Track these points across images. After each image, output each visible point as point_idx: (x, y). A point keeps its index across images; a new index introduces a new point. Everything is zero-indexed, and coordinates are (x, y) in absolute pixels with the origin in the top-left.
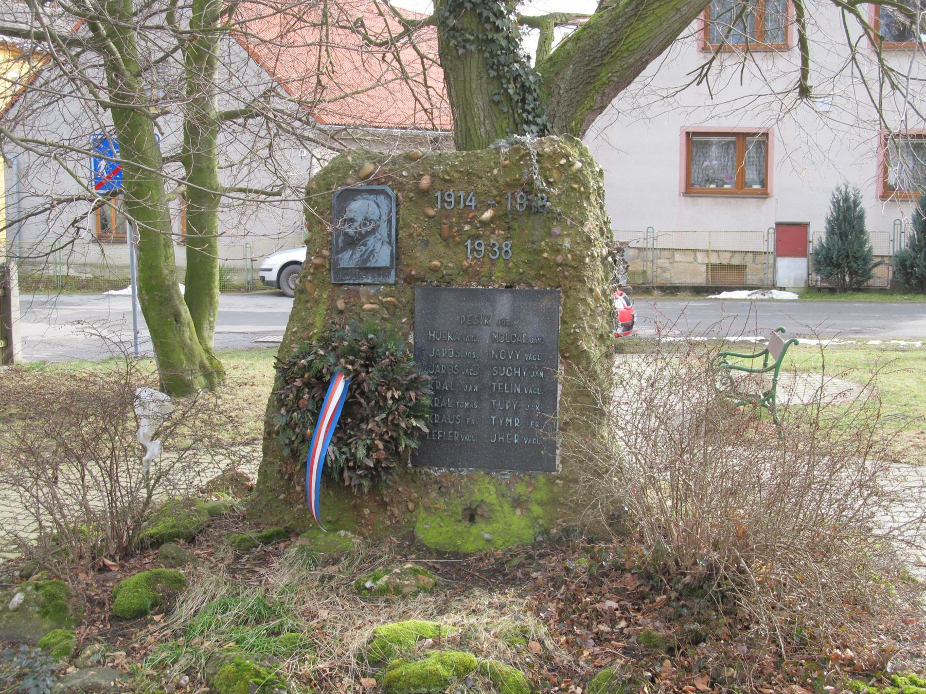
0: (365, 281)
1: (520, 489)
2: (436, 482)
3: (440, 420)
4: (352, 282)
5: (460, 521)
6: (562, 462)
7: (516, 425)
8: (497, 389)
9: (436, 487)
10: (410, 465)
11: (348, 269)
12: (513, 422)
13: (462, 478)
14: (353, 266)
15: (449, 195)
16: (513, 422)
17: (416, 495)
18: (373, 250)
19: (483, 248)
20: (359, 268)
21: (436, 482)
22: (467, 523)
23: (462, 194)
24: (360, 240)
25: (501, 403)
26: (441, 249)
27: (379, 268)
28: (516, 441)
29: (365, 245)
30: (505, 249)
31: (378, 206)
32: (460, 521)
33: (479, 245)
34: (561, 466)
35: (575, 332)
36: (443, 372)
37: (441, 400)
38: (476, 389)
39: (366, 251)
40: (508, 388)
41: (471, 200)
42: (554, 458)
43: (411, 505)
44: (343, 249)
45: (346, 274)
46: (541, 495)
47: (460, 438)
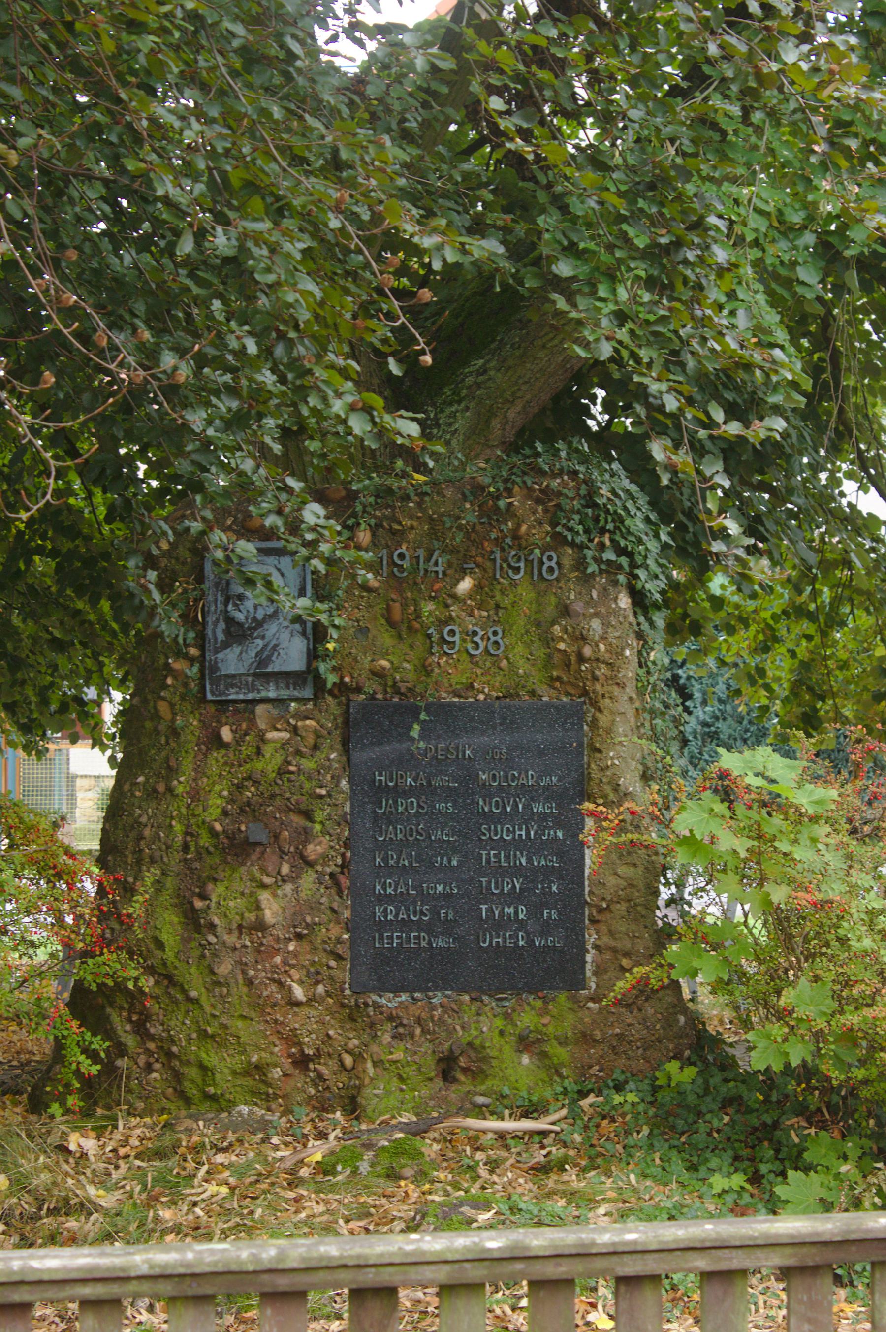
0: (263, 694)
1: (527, 1020)
2: (391, 1018)
3: (397, 915)
4: (241, 697)
5: (431, 1079)
6: (595, 973)
7: (521, 916)
8: (488, 861)
9: (388, 1026)
10: (348, 992)
11: (234, 676)
12: (516, 913)
13: (434, 1008)
14: (242, 671)
15: (402, 556)
16: (516, 913)
17: (356, 1042)
18: (276, 645)
19: (457, 638)
20: (255, 675)
21: (391, 1018)
22: (439, 1083)
23: (421, 553)
24: (255, 629)
25: (496, 883)
26: (387, 639)
27: (287, 674)
28: (521, 943)
29: (263, 637)
30: (493, 639)
31: (282, 575)
32: (431, 1079)
33: (452, 633)
34: (594, 979)
35: (613, 764)
36: (400, 836)
37: (397, 885)
38: (454, 863)
39: (265, 646)
40: (507, 857)
41: (436, 564)
42: (583, 967)
43: (348, 1060)
44: (226, 645)
45: (233, 686)
46: (568, 1025)
47: (430, 943)
